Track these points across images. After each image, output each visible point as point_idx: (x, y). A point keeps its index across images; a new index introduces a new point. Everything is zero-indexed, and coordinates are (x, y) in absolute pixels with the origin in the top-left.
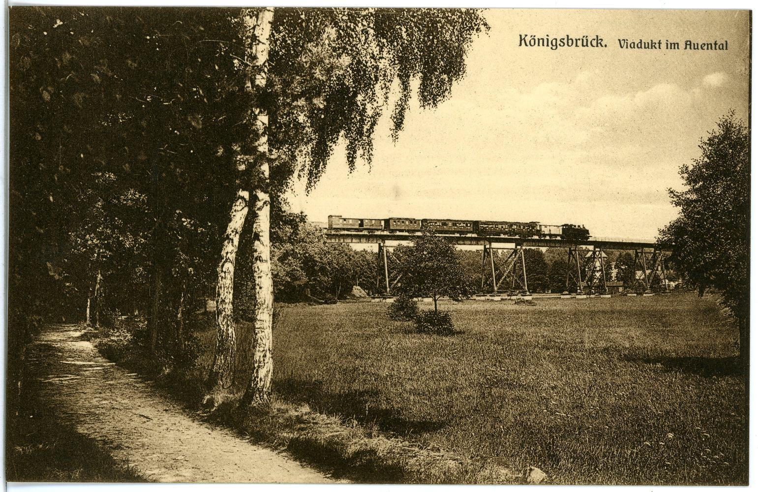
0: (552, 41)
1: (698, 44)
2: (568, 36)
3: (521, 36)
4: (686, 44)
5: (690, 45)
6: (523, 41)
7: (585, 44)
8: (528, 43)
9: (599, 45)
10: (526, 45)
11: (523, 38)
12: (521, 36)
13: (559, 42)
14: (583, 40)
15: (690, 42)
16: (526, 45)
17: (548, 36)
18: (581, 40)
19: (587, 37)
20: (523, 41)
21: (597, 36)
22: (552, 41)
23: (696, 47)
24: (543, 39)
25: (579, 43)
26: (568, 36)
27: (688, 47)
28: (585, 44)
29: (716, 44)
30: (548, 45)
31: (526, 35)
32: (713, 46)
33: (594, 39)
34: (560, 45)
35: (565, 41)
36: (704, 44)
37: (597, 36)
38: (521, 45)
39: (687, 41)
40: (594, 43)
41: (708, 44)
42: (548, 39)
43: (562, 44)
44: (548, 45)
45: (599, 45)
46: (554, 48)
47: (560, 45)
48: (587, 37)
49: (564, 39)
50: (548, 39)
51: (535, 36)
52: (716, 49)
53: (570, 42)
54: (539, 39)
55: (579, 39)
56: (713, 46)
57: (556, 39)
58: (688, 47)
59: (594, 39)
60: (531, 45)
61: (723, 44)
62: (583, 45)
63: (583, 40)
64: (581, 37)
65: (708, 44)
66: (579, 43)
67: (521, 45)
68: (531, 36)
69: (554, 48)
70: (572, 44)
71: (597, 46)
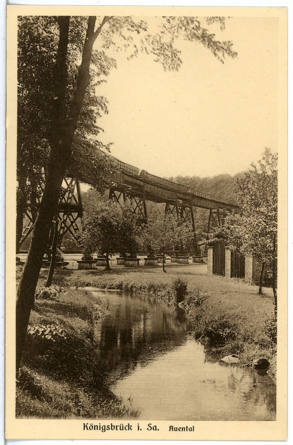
0: (102, 427)
1: (177, 428)
2: (112, 424)
3: (84, 424)
4: (170, 428)
5: (173, 428)
6: (86, 427)
7: (122, 429)
8: (88, 428)
9: (130, 429)
10: (87, 429)
11: (85, 425)
12: (84, 424)
13: (106, 428)
14: (120, 426)
15: (173, 427)
16: (87, 429)
17: (100, 424)
18: (119, 427)
19: (123, 424)
20: (86, 427)
21: (129, 424)
22: (102, 427)
23: (176, 430)
24: (97, 426)
25: (118, 428)
26: (112, 424)
27: (171, 429)
28: (122, 429)
29: (187, 428)
30: (100, 429)
31: (87, 424)
32: (186, 429)
33: (127, 426)
34: (107, 429)
35: (110, 427)
36: (180, 428)
37: (129, 424)
38: (84, 429)
39: (171, 426)
40: (127, 428)
41: (182, 428)
42: (100, 426)
43: (108, 429)
44: (100, 429)
45: (130, 429)
46: (104, 431)
47: (107, 429)
48: (123, 424)
49: (109, 426)
50: (100, 426)
51: (92, 424)
52: (187, 430)
53: (113, 427)
54: (95, 426)
55: (118, 426)
56: (186, 429)
57: (105, 426)
58: (171, 429)
59: (127, 426)
60: (90, 429)
61: (191, 428)
62: (120, 429)
63: (120, 426)
64: (119, 425)
65: (182, 428)
66: (118, 428)
67: (84, 429)
68: (90, 424)
69: (104, 431)
70: (92, 428)
71: (129, 430)
